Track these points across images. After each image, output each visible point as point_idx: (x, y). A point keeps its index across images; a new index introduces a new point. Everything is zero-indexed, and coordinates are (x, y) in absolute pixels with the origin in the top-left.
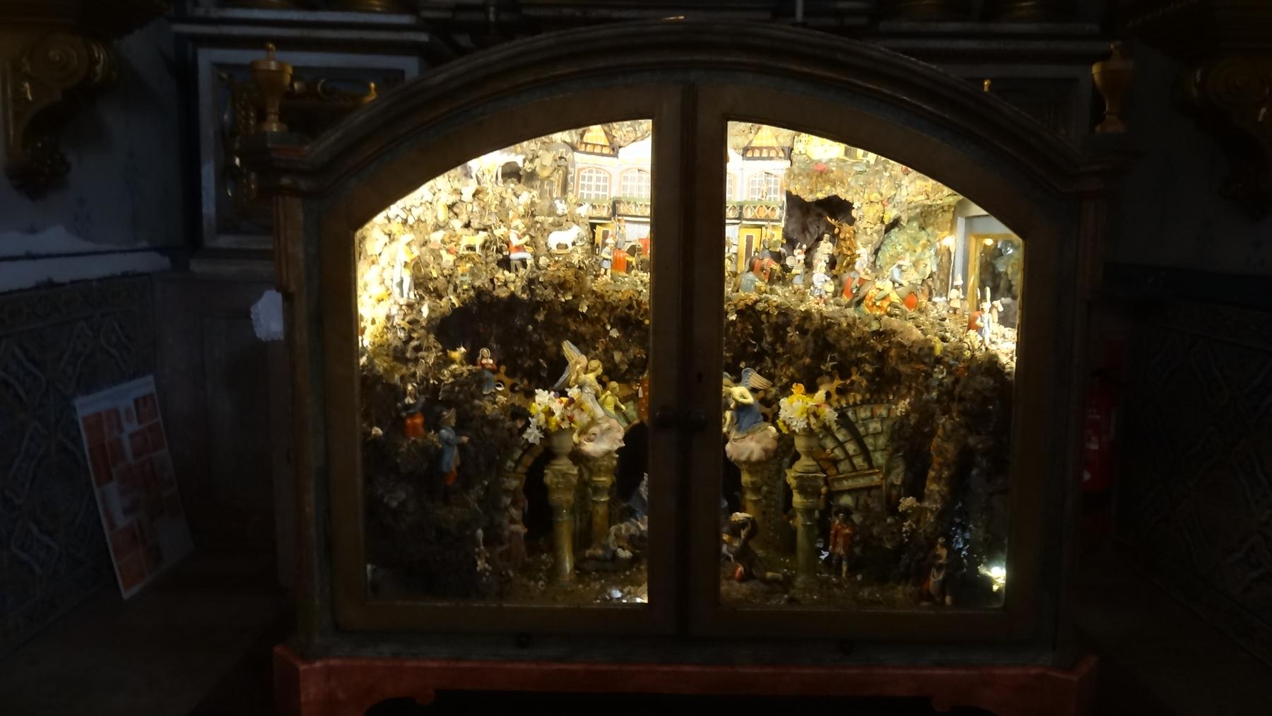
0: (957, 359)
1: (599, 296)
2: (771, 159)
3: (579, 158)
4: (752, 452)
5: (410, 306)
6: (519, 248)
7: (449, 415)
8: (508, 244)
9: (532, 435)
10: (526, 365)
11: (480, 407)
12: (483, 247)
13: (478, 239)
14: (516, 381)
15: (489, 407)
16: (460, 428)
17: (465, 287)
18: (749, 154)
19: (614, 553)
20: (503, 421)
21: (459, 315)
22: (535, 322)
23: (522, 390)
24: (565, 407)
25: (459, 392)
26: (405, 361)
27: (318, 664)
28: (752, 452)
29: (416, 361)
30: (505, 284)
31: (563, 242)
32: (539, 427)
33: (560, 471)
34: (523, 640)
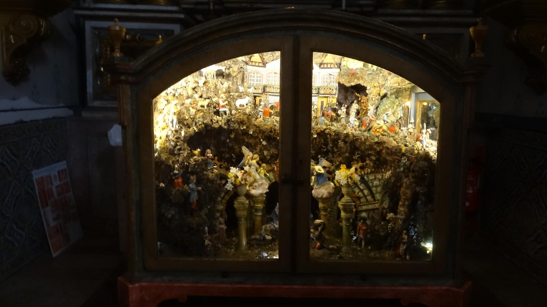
0: (412, 154)
1: (257, 127)
2: (332, 68)
3: (249, 68)
4: (323, 194)
5: (176, 131)
6: (223, 106)
7: (193, 178)
8: (219, 104)
9: (229, 187)
10: (226, 157)
11: (207, 174)
12: (208, 106)
13: (206, 103)
14: (222, 163)
15: (210, 175)
16: (198, 183)
17: (200, 123)
18: (322, 66)
19: (264, 237)
20: (216, 180)
21: (197, 135)
22: (230, 138)
23: (224, 167)
24: (243, 175)
25: (197, 168)
26: (174, 155)
27: (137, 285)
28: (323, 194)
29: (179, 155)
30: (217, 122)
31: (242, 104)
32: (232, 183)
33: (241, 202)
34: (225, 274)
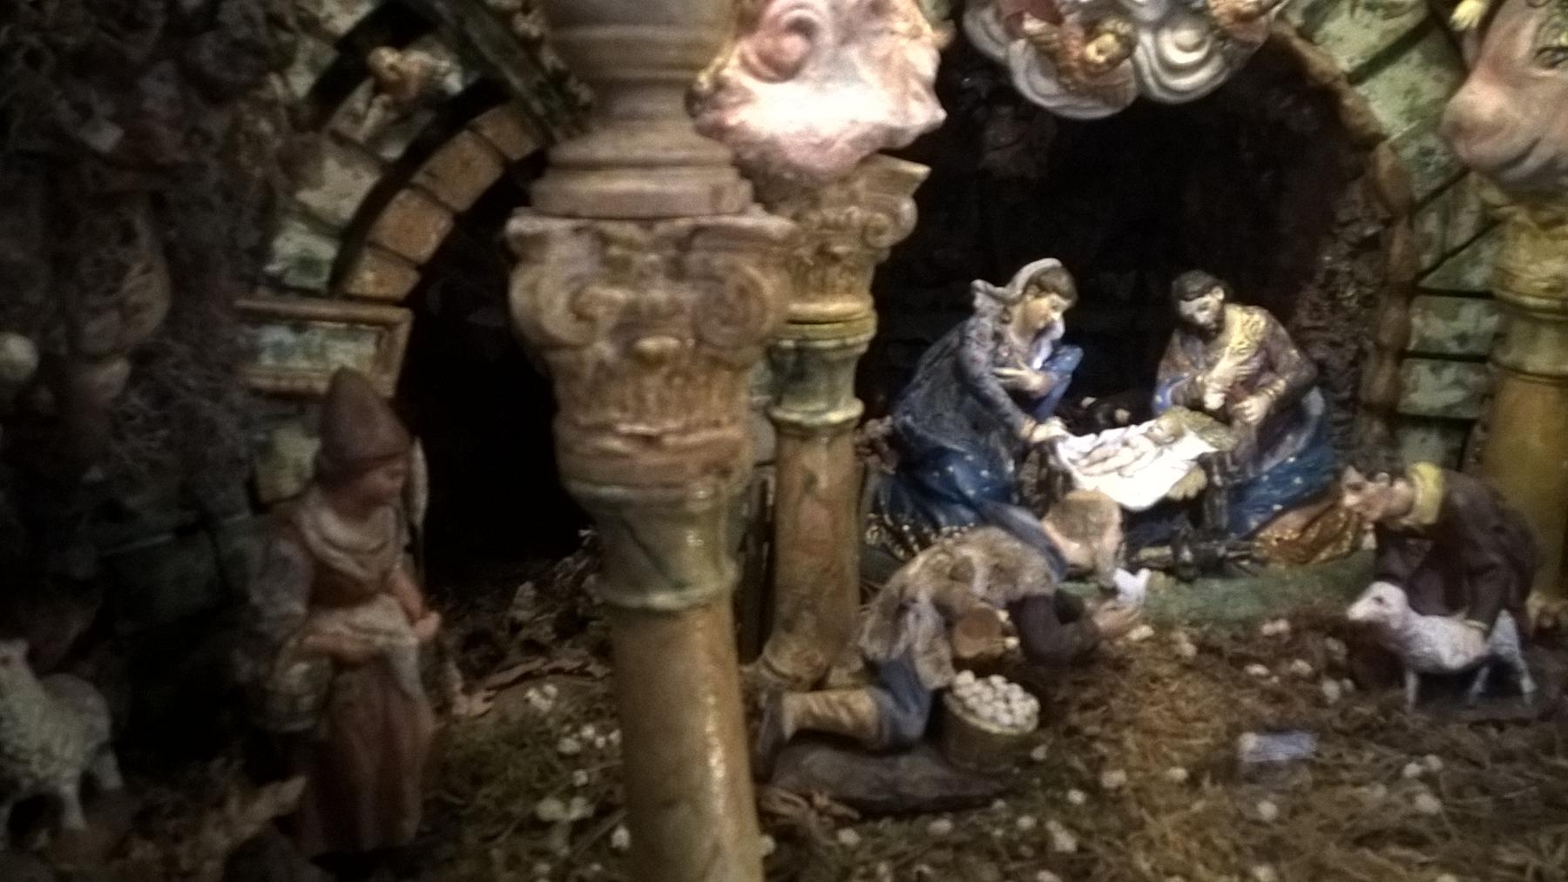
19: (942, 717)
